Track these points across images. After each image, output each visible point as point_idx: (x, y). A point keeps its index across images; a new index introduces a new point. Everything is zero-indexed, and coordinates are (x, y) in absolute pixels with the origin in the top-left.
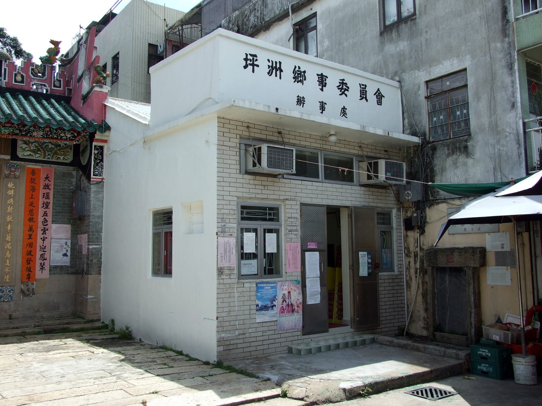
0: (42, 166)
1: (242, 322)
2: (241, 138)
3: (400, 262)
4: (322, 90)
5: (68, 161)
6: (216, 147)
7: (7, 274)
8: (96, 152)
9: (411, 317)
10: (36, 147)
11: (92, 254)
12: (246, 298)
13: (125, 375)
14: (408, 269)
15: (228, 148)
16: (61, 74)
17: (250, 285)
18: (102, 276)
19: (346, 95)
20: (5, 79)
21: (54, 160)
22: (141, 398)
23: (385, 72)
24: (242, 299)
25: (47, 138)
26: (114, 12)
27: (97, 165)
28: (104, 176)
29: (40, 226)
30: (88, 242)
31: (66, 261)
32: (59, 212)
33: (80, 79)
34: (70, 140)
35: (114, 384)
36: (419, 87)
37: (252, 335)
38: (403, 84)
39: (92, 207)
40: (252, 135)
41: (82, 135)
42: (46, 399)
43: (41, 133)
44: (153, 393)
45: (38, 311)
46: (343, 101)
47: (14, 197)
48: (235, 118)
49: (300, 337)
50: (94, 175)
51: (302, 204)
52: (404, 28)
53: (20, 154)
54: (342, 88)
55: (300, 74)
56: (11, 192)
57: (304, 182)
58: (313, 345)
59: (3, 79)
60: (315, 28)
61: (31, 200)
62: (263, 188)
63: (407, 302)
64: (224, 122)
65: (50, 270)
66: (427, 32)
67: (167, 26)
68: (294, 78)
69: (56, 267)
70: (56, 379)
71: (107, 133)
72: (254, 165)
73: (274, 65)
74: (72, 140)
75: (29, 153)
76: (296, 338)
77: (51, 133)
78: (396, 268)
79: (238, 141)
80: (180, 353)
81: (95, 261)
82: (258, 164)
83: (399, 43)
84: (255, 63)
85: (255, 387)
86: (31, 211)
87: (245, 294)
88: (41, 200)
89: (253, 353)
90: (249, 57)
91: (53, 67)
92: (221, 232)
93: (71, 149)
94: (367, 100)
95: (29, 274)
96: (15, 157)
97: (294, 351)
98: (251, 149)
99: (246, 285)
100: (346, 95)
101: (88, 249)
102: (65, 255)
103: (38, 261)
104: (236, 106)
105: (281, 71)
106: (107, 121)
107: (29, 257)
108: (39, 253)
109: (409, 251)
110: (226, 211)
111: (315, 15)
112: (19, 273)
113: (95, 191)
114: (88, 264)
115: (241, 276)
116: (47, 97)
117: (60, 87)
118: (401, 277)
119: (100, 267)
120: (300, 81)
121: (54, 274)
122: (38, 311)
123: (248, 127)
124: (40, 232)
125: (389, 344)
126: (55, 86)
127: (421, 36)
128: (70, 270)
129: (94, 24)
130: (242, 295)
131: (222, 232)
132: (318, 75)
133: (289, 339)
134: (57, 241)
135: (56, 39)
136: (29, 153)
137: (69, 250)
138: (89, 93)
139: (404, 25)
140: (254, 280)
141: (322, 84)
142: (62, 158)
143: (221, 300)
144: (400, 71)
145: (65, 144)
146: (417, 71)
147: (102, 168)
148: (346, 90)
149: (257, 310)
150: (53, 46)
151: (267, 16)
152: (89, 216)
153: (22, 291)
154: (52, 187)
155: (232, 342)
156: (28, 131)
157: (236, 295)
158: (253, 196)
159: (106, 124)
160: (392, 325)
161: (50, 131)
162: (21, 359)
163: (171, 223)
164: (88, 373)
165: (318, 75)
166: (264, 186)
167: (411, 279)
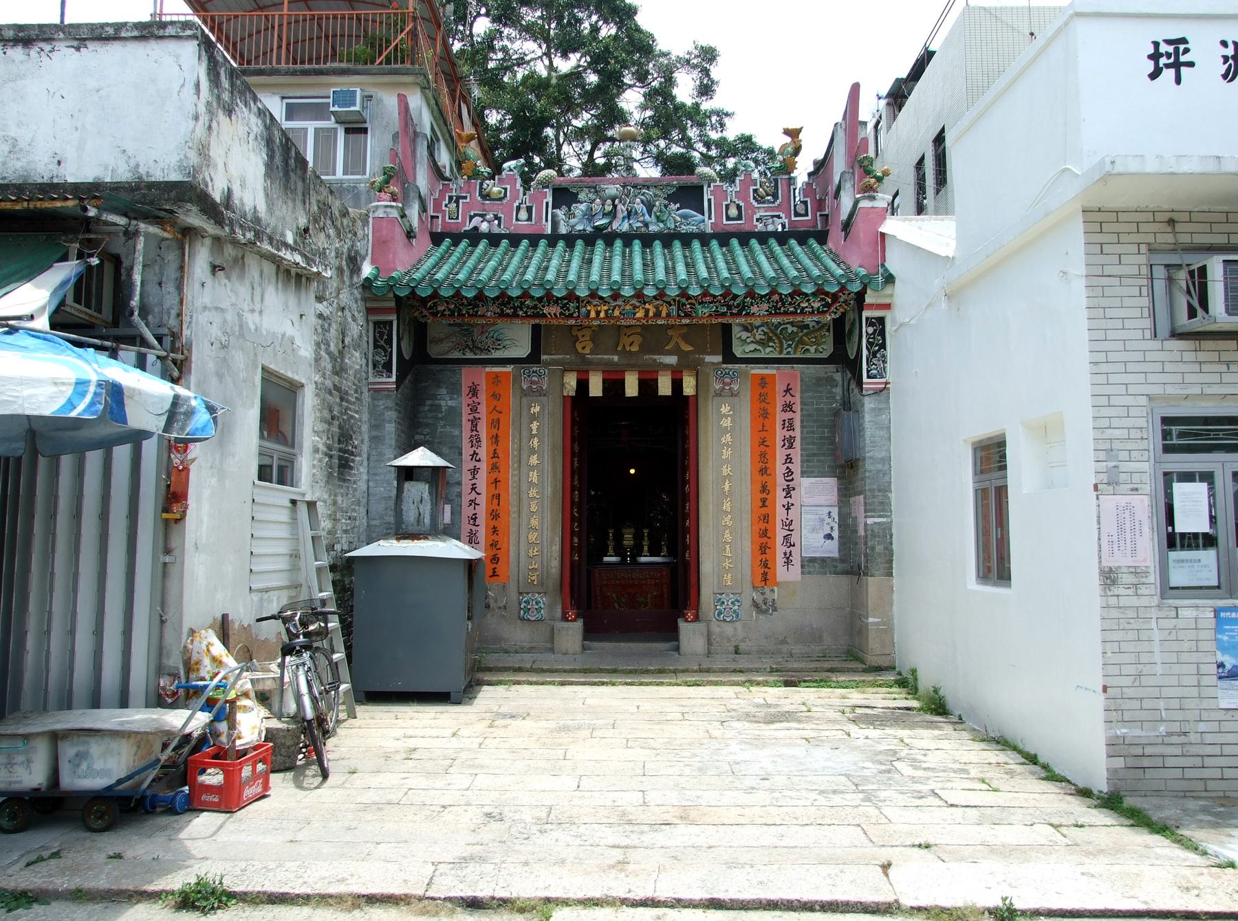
0: (778, 369)
1: (1175, 704)
5: (825, 355)
6: (1083, 282)
7: (727, 572)
8: (871, 330)
10: (765, 333)
11: (874, 536)
12: (1186, 646)
13: (882, 795)
15: (1116, 281)
16: (808, 186)
17: (1198, 613)
18: (895, 581)
20: (710, 218)
21: (798, 355)
22: (885, 855)
24: (1175, 646)
26: (931, 48)
27: (874, 355)
28: (889, 377)
29: (781, 482)
30: (865, 511)
31: (831, 549)
32: (814, 455)
34: (819, 312)
35: (850, 809)
37: (1209, 738)
39: (867, 442)
40: (1185, 239)
41: (841, 300)
42: (709, 821)
43: (765, 306)
44: (920, 846)
45: (784, 642)
47: (732, 431)
48: (1133, 205)
50: (869, 377)
53: (738, 351)
56: (727, 423)
61: (763, 434)
62: (1223, 368)
64: (1102, 221)
65: (802, 567)
69: (812, 560)
70: (749, 782)
71: (888, 290)
72: (1192, 314)
75: (752, 347)
77: (783, 305)
79: (1142, 259)
80: (1032, 759)
81: (879, 549)
82: (1200, 312)
84: (1183, 59)
85: (1184, 877)
86: (763, 455)
87: (1181, 635)
88: (780, 434)
91: (790, 179)
92: (1108, 483)
93: (828, 330)
95: (765, 574)
96: (729, 357)
98: (1182, 276)
101: (866, 524)
102: (829, 537)
103: (780, 549)
104: (1119, 174)
107: (764, 540)
108: (780, 533)
110: (1117, 433)
112: (747, 571)
113: (873, 410)
114: (866, 555)
115: (1168, 590)
116: (782, 238)
117: (806, 215)
119: (891, 561)
121: (809, 573)
122: (784, 642)
123: (1171, 222)
124: (780, 494)
126: (797, 214)
128: (840, 567)
129: (899, 82)
130: (1173, 637)
131: (1108, 484)
134: (813, 508)
135: (792, 126)
136: (752, 347)
137: (836, 527)
140: (1210, 602)
142: (812, 349)
143: (1115, 647)
145: (818, 322)
149: (1220, 678)
150: (788, 140)
152: (864, 459)
153: (755, 605)
154: (797, 407)
155: (1149, 750)
156: (743, 306)
157: (1157, 635)
158: (1196, 390)
162: (716, 731)
164: (815, 779)
166: (1228, 363)
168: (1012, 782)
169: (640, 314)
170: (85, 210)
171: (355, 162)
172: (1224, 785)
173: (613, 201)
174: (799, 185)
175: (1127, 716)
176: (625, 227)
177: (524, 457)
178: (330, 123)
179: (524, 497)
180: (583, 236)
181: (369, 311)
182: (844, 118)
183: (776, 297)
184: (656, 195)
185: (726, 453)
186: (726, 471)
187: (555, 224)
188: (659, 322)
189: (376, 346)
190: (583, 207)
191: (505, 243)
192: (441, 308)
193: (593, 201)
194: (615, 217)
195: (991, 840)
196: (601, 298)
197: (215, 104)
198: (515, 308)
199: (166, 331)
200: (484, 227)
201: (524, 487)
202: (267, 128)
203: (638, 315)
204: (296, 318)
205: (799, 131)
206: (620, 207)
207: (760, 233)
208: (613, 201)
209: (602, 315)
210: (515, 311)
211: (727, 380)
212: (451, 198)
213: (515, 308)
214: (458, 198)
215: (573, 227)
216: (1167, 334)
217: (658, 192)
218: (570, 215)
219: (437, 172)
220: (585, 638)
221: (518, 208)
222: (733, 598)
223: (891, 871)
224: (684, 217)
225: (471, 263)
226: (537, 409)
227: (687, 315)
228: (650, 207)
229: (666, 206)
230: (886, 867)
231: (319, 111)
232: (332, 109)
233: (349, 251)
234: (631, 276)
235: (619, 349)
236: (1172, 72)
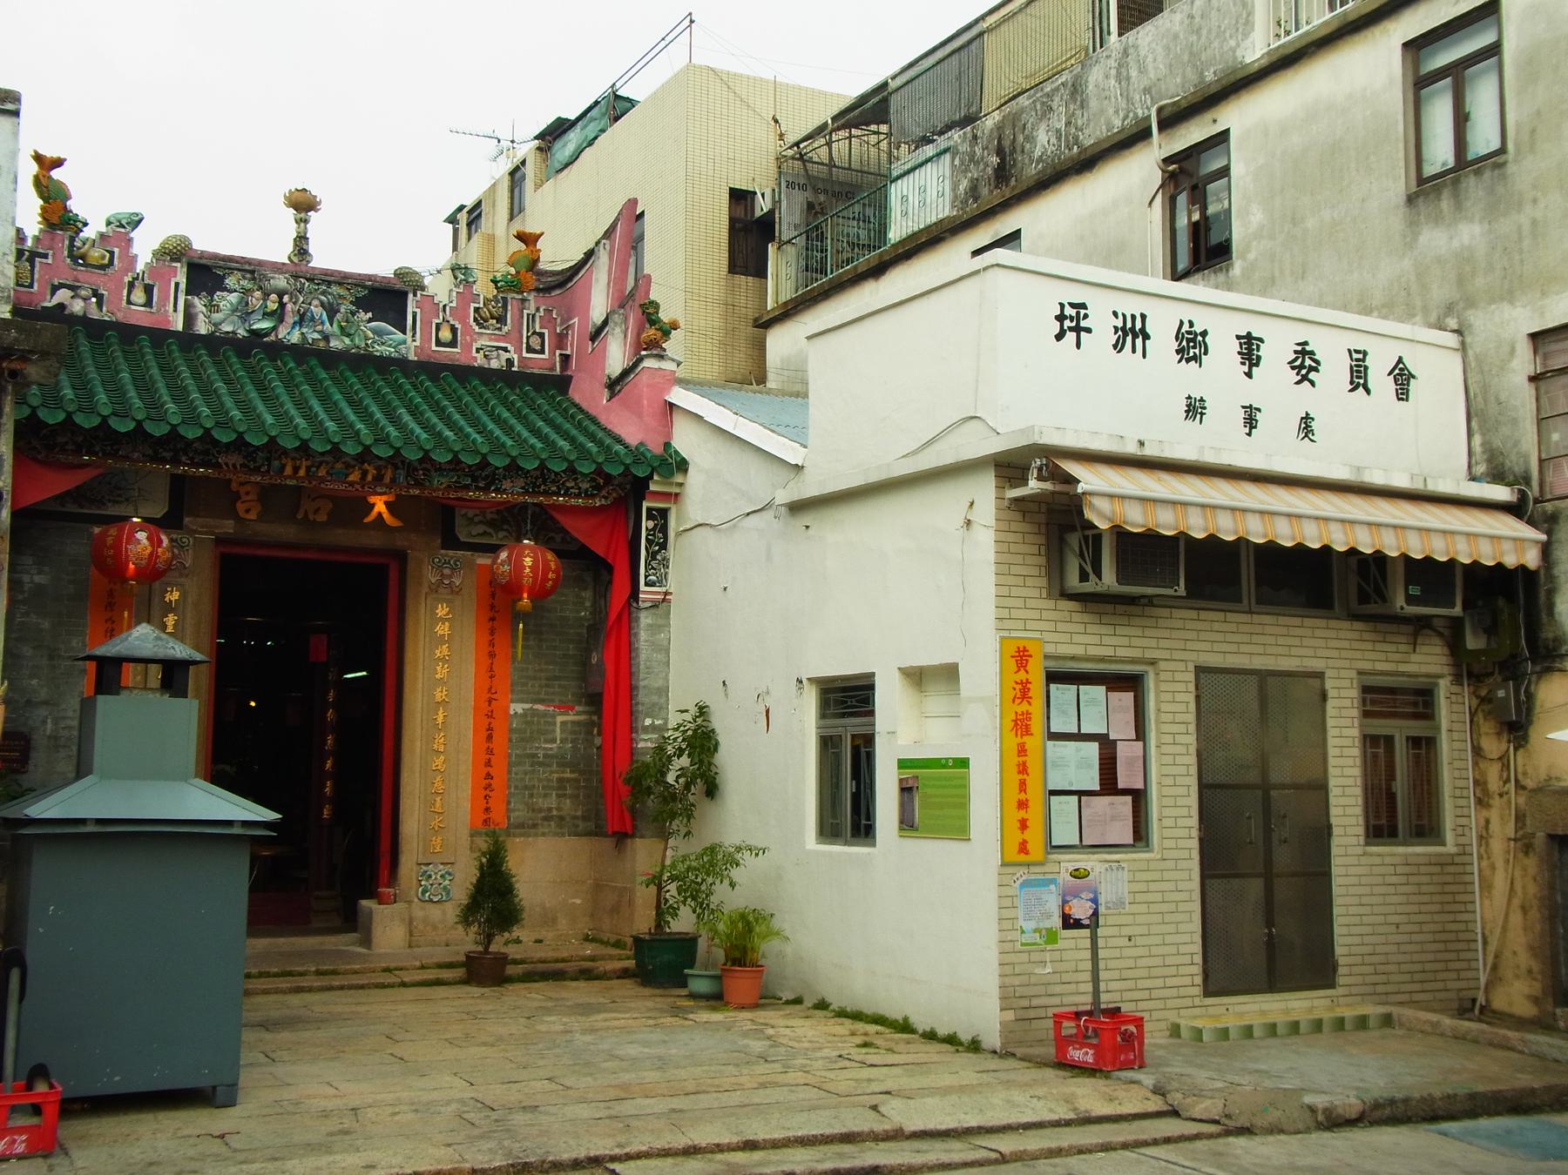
2: (1050, 511)
3: (1464, 821)
4: (1249, 375)
8: (651, 524)
9: (1495, 967)
14: (1484, 838)
19: (1312, 383)
23: (1418, 303)
27: (654, 558)
28: (672, 585)
32: (556, 678)
33: (597, 333)
36: (1513, 351)
38: (1468, 340)
46: (1306, 399)
49: (1197, 1001)
50: (647, 584)
51: (1200, 670)
52: (1474, 187)
54: (1302, 366)
55: (1193, 340)
56: (443, 629)
57: (1204, 615)
58: (1232, 1022)
59: (409, 340)
60: (1225, 172)
63: (1483, 928)
66: (1535, 201)
67: (781, 136)
68: (1178, 352)
71: (679, 478)
72: (1084, 577)
73: (1129, 325)
74: (593, 496)
76: (1188, 1002)
78: (1449, 836)
83: (1460, 226)
84: (1083, 324)
90: (1069, 311)
94: (1368, 391)
97: (1184, 1033)
100: (1312, 383)
105: (1146, 337)
109: (1486, 792)
111: (1223, 137)
113: (650, 626)
117: (542, 352)
118: (1466, 859)
120: (1195, 358)
125: (1430, 1029)
126: (530, 350)
127: (1519, 212)
132: (1238, 337)
133: (1170, 1003)
138: (626, 373)
139: (1472, 180)
141: (1250, 360)
144: (1461, 305)
146: (1506, 306)
148: (1311, 369)
151: (1087, 132)
155: (1035, 1002)
160: (1440, 985)
163: (872, 713)
165: (1238, 337)
167: (1493, 867)
173: (281, 297)
175: (1017, 971)
176: (295, 338)
184: (340, 297)
185: (441, 671)
186: (439, 695)
187: (189, 318)
190: (233, 298)
193: (247, 292)
194: (281, 320)
200: (77, 307)
203: (351, 478)
206: (289, 307)
207: (481, 369)
208: (281, 297)
211: (447, 571)
215: (215, 325)
217: (342, 292)
218: (212, 307)
221: (131, 285)
224: (378, 333)
226: (175, 596)
227: (418, 484)
228: (332, 311)
229: (353, 314)
235: (299, 516)
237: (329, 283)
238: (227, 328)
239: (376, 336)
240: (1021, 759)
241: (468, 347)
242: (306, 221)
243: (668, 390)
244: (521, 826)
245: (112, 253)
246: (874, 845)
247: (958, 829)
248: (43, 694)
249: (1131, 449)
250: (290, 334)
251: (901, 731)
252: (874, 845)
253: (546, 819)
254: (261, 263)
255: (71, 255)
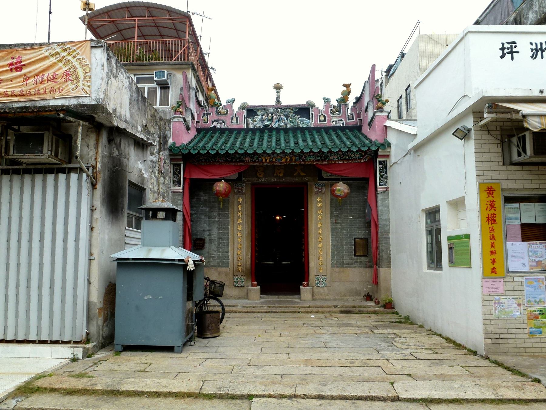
2: (502, 130)
8: (381, 166)
18: (392, 270)
25: (341, 160)
27: (382, 177)
32: (357, 218)
43: (336, 157)
50: (380, 185)
56: (320, 205)
71: (388, 150)
72: (519, 155)
74: (361, 159)
81: (385, 256)
82: (523, 154)
84: (514, 50)
89: (528, 350)
91: (346, 105)
99: (516, 279)
106: (388, 139)
116: (343, 129)
117: (353, 119)
119: (390, 262)
122: (345, 295)
126: (349, 119)
147: (387, 179)
150: (345, 88)
155: (502, 336)
156: (327, 157)
159: (387, 141)
161: (343, 154)
168: (444, 350)
169: (284, 160)
170: (59, 115)
171: (164, 101)
172: (533, 350)
173: (272, 115)
174: (350, 107)
176: (277, 125)
177: (235, 219)
178: (154, 85)
179: (236, 236)
180: (259, 129)
181: (171, 160)
182: (369, 79)
183: (341, 153)
184: (290, 112)
185: (320, 218)
187: (248, 125)
188: (292, 164)
189: (174, 174)
190: (260, 117)
191: (227, 132)
192: (201, 159)
193: (263, 115)
194: (273, 121)
195: (436, 373)
196: (268, 154)
197: (110, 74)
198: (232, 158)
199: (90, 165)
200: (219, 126)
201: (236, 232)
202: (130, 84)
203: (283, 161)
204: (142, 160)
205: (350, 85)
207: (334, 127)
208: (272, 115)
209: (268, 161)
210: (232, 159)
211: (320, 188)
212: (204, 114)
213: (232, 158)
214: (208, 114)
215: (255, 126)
216: (509, 163)
217: (290, 111)
218: (254, 120)
219: (198, 102)
220: (261, 294)
221: (232, 118)
222: (323, 277)
223: (394, 385)
225: (213, 140)
226: (241, 200)
227: (303, 161)
228: (287, 117)
229: (294, 117)
230: (392, 384)
231: (150, 80)
232: (155, 79)
233: (163, 135)
234: (280, 145)
235: (275, 175)
236: (510, 55)
237: (286, 109)
238: (258, 126)
239: (302, 122)
240: (492, 234)
241: (329, 121)
242: (279, 92)
243: (385, 122)
244: (348, 264)
245: (227, 110)
246: (442, 270)
247: (468, 264)
248: (208, 228)
249: (536, 94)
250: (275, 125)
251: (449, 227)
252: (442, 270)
253: (355, 262)
254: (267, 106)
255: (217, 112)
